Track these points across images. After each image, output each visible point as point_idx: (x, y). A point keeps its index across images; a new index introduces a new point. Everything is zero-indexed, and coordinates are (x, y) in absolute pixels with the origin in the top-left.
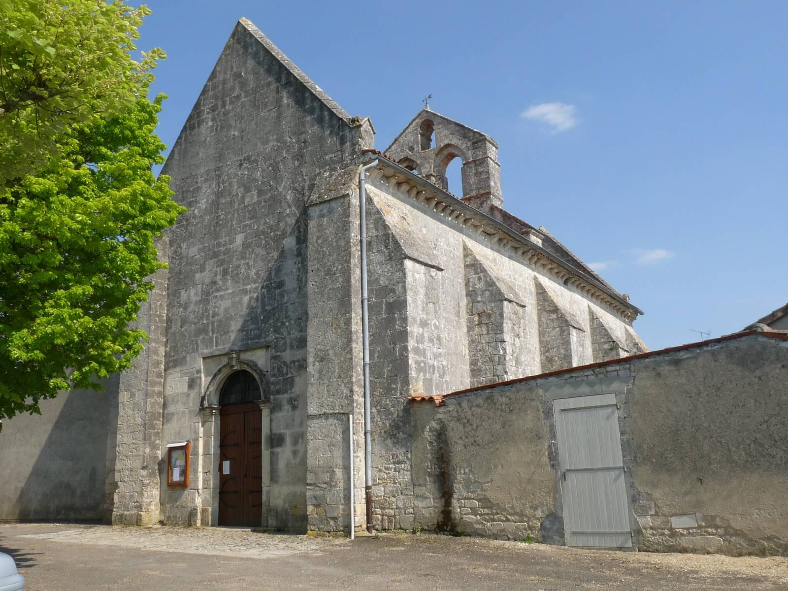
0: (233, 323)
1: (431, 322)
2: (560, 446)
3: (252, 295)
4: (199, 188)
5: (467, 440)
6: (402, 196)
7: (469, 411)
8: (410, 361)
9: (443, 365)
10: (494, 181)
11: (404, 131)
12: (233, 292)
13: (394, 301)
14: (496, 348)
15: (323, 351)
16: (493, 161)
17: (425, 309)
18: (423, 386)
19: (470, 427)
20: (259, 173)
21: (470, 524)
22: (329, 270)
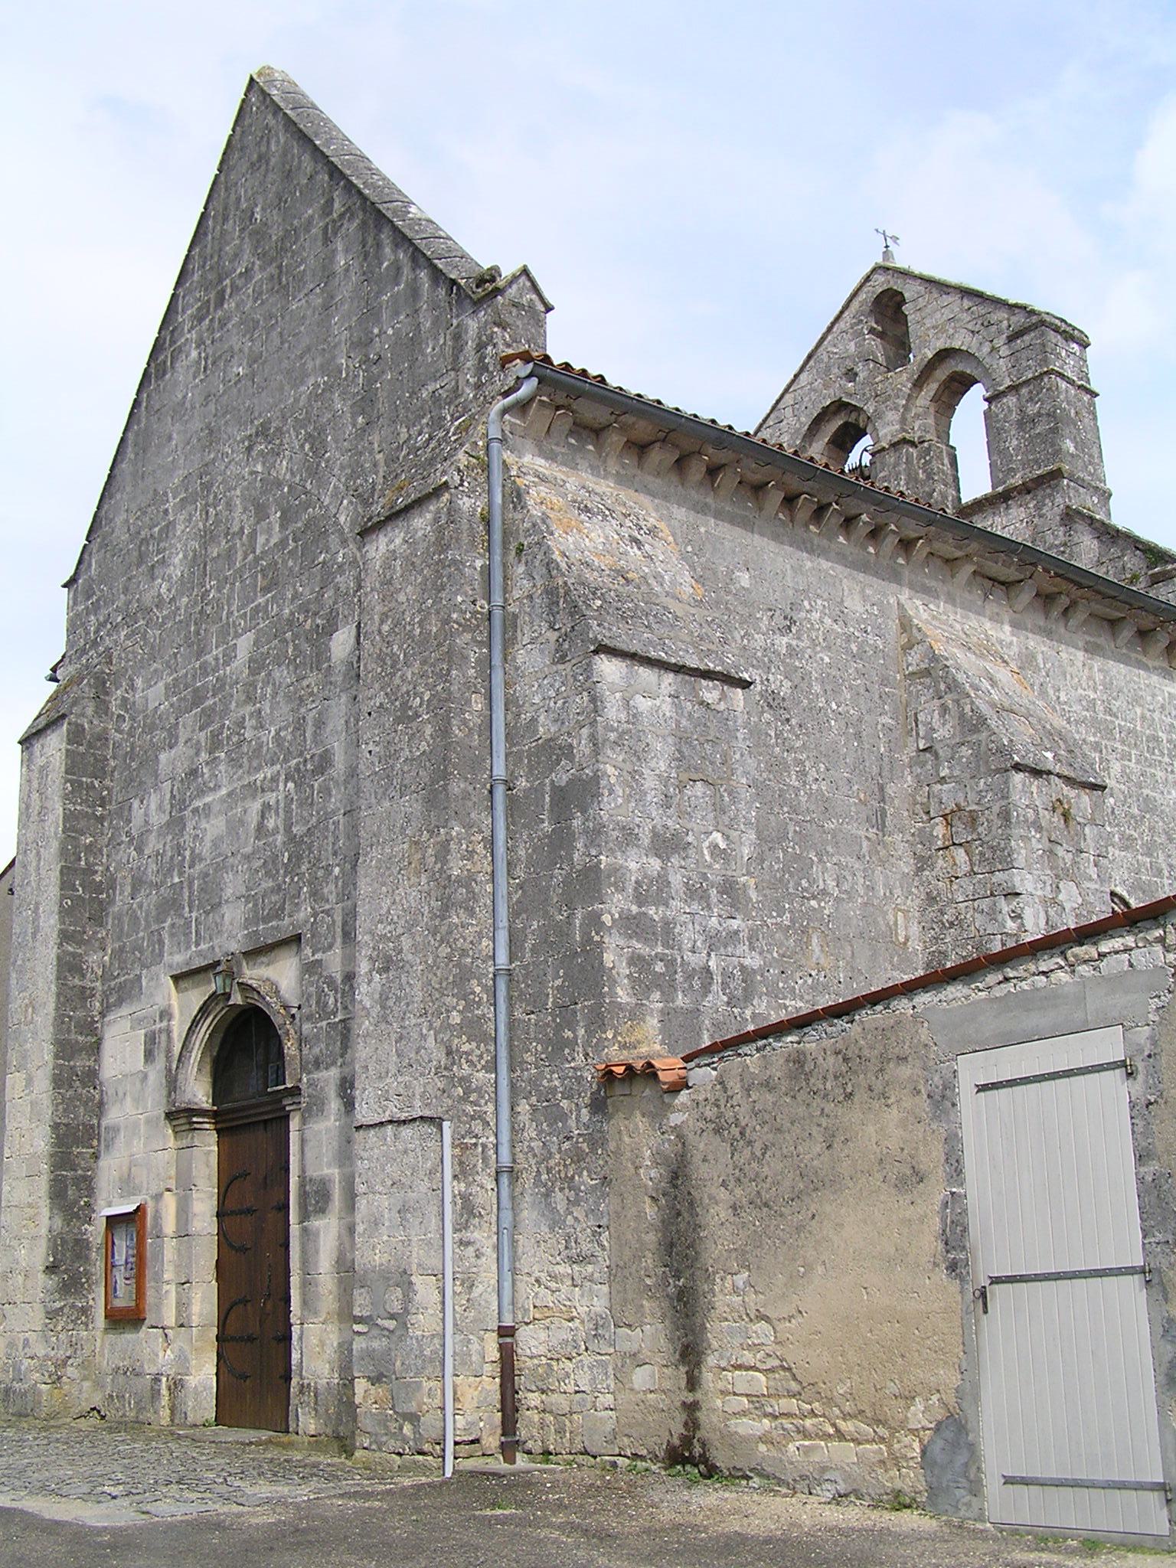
0: (228, 877)
1: (700, 842)
2: (971, 1202)
3: (266, 799)
4: (171, 525)
5: (738, 1191)
6: (655, 483)
7: (743, 1103)
8: (609, 958)
9: (743, 968)
10: (1074, 440)
11: (830, 329)
12: (229, 795)
13: (570, 782)
14: (993, 914)
15: (389, 939)
16: (1071, 382)
17: (676, 800)
18: (661, 1031)
19: (747, 1152)
20: (284, 463)
21: (734, 1442)
22: (405, 706)
